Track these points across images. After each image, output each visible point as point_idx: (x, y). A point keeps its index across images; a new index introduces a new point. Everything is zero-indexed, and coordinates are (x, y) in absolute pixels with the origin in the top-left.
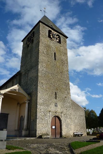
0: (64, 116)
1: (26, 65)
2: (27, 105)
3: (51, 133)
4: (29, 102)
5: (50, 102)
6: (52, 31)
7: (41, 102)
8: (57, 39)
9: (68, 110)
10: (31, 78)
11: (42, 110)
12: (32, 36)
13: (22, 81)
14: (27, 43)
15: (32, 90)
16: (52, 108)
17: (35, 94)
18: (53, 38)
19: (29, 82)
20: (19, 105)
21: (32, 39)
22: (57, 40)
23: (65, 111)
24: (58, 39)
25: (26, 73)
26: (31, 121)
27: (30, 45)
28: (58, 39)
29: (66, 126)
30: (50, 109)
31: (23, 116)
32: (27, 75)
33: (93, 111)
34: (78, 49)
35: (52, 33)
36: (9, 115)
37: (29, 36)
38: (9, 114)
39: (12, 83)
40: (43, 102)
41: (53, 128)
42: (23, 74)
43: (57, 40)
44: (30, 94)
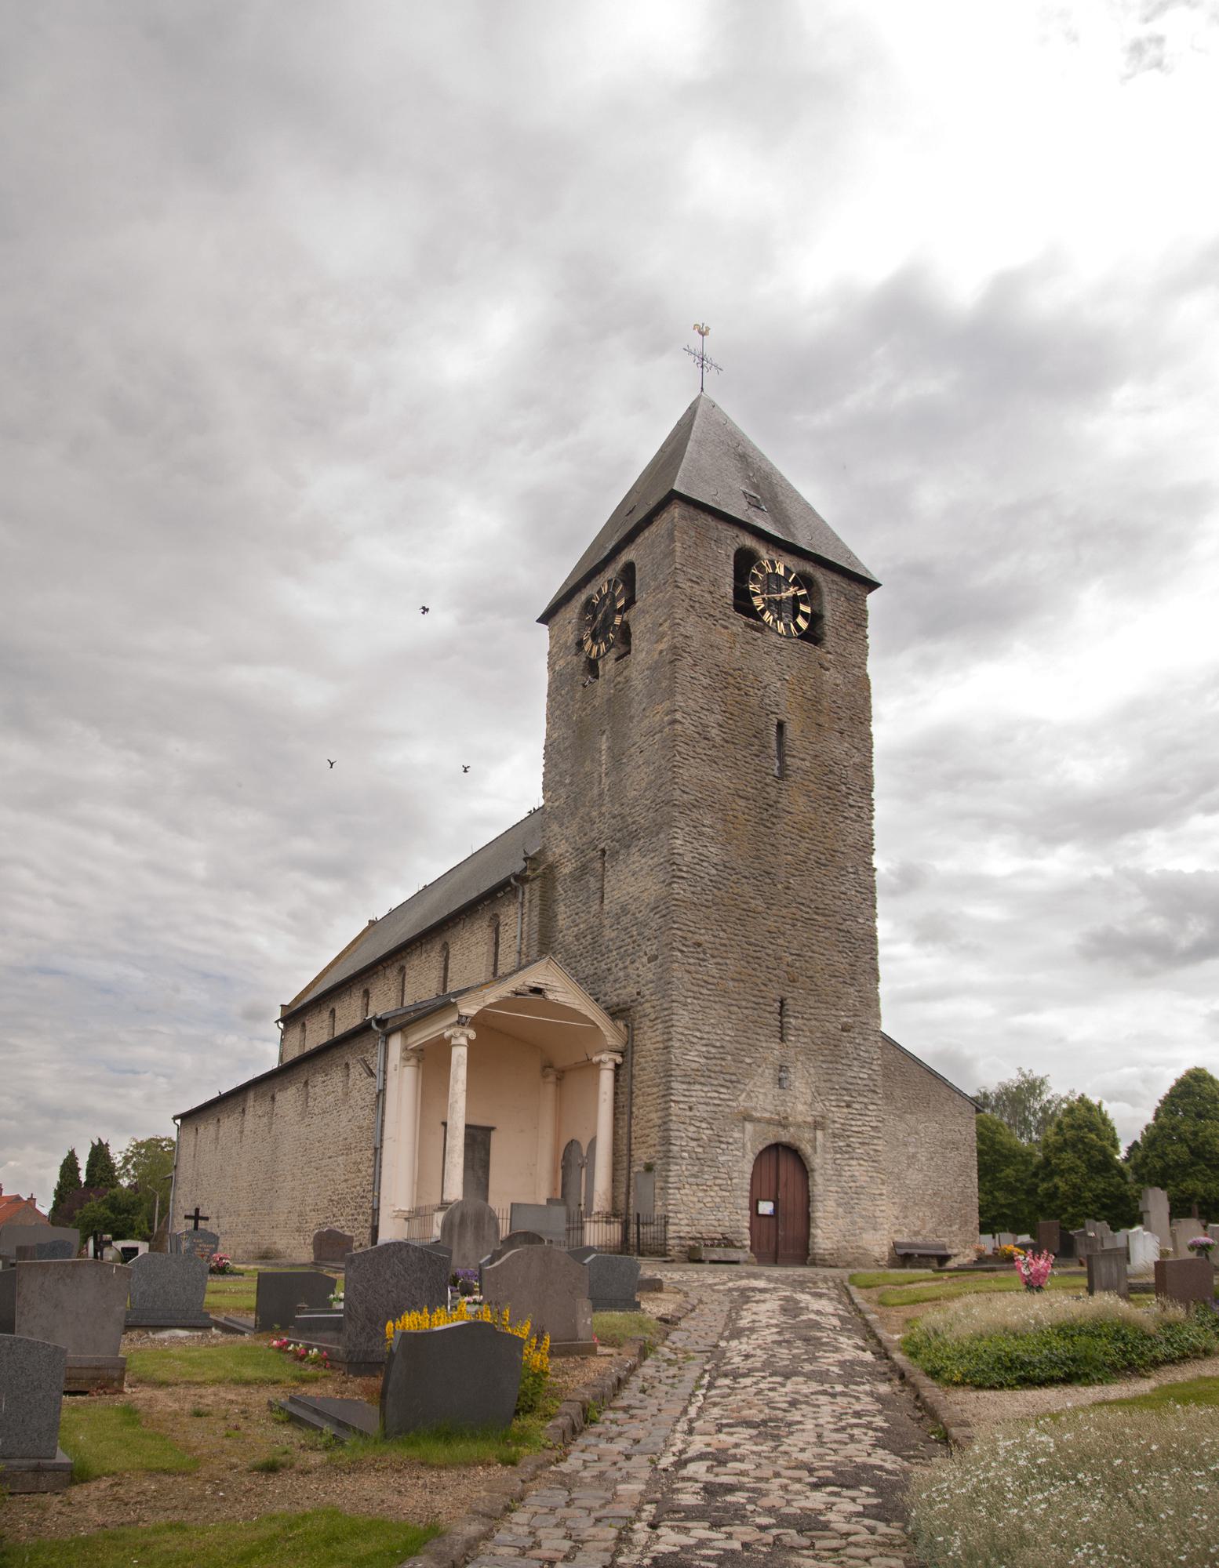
0: (829, 1144)
1: (582, 810)
2: (606, 1079)
3: (748, 1236)
4: (619, 1060)
5: (748, 1060)
6: (760, 558)
7: (694, 1066)
8: (796, 612)
9: (855, 1106)
10: (624, 910)
11: (701, 1111)
12: (614, 600)
13: (562, 921)
14: (580, 644)
15: (632, 990)
16: (761, 1097)
17: (653, 1016)
18: (767, 614)
19: (609, 934)
20: (552, 1078)
21: (618, 620)
22: (795, 617)
23: (838, 1115)
24: (802, 608)
25: (584, 869)
26: (636, 1169)
27: (607, 667)
28: (807, 609)
29: (839, 1205)
30: (742, 1102)
31: (578, 1143)
32: (593, 884)
33: (1089, 1108)
34: (875, 870)
35: (761, 569)
36: (493, 1134)
37: (590, 590)
38: (493, 1129)
39: (485, 924)
40: (702, 1061)
41: (761, 1211)
42: (566, 871)
43: (800, 621)
44: (623, 1010)
